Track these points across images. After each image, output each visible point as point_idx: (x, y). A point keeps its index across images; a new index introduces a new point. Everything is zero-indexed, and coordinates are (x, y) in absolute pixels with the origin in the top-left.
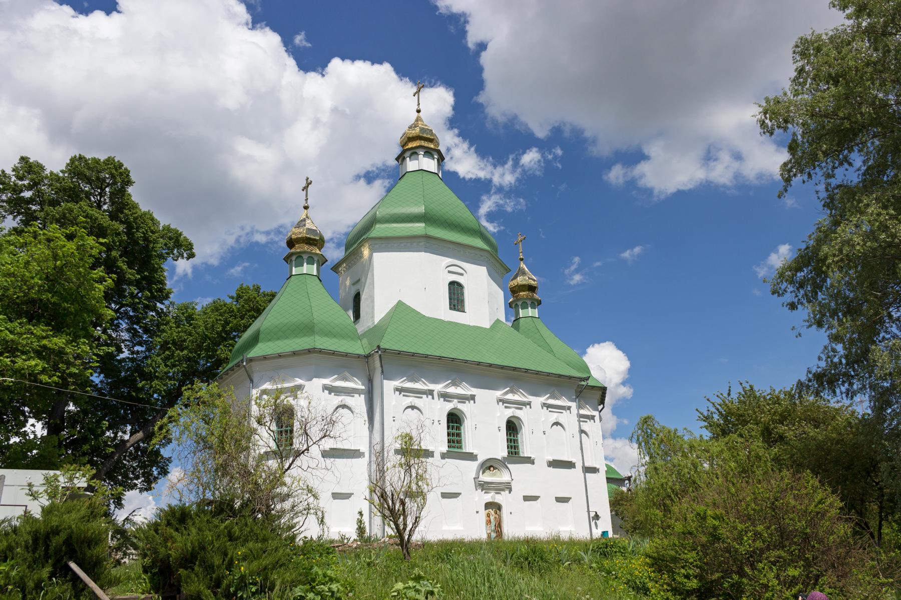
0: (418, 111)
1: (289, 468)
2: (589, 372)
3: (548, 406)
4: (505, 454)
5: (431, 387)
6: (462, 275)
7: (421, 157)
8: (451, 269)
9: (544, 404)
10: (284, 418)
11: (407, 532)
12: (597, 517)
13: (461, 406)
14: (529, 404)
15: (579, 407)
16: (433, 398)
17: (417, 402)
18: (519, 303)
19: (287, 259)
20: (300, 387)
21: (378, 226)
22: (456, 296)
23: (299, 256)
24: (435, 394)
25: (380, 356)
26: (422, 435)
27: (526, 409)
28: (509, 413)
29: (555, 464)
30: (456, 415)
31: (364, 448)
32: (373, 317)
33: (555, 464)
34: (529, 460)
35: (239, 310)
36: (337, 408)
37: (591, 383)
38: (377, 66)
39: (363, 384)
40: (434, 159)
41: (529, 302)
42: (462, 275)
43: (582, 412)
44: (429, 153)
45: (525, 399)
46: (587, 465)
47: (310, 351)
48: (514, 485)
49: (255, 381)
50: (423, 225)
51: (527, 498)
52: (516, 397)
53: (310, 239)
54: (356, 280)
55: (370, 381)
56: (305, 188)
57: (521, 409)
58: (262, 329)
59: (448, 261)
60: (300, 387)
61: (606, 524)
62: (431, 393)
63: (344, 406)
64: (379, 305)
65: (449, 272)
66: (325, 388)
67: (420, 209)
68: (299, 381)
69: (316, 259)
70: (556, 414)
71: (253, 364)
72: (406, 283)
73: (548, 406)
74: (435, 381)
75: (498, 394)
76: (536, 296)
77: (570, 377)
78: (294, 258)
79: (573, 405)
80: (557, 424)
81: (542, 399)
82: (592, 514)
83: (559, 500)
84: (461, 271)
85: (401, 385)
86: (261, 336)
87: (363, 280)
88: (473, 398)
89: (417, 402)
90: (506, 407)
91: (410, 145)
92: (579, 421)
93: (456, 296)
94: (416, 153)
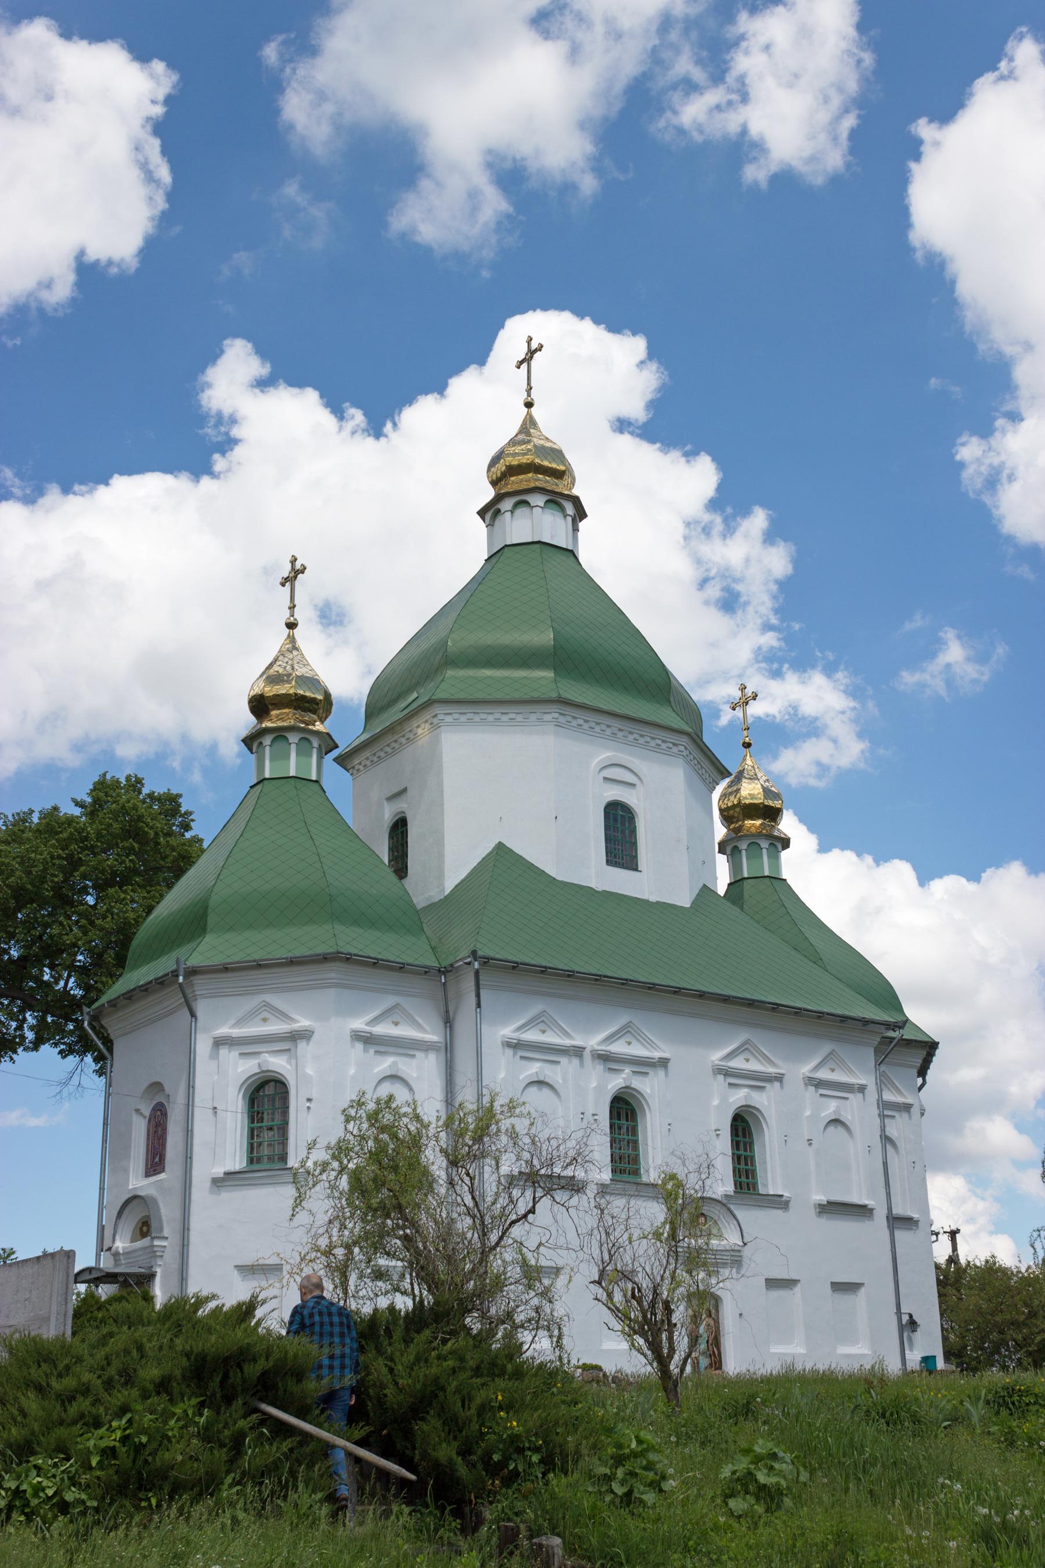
0: (529, 405)
1: (497, 1244)
2: (898, 1007)
4: (729, 1188)
5: (578, 1042)
6: (633, 785)
8: (611, 773)
10: (267, 1099)
11: (677, 1358)
12: (913, 1324)
13: (637, 1083)
14: (779, 1078)
15: (883, 1082)
17: (553, 1074)
18: (743, 845)
19: (251, 741)
20: (305, 1035)
21: (450, 673)
22: (620, 830)
23: (280, 734)
24: (587, 1054)
25: (477, 973)
26: (708, 1182)
27: (773, 1089)
28: (739, 1097)
29: (833, 1209)
30: (627, 1103)
33: (833, 1209)
34: (779, 1202)
35: (99, 836)
37: (907, 1034)
38: (947, 886)
39: (433, 1033)
40: (752, 716)
42: (633, 785)
43: (888, 1096)
45: (771, 1070)
46: (897, 1211)
47: (325, 958)
48: (746, 1252)
49: (202, 1007)
50: (550, 674)
51: (772, 1283)
52: (638, 1050)
53: (303, 697)
54: (396, 789)
55: (448, 1022)
57: (761, 1088)
58: (212, 903)
59: (606, 755)
60: (305, 1035)
61: (929, 1342)
62: (578, 1052)
63: (540, 1083)
66: (359, 1037)
67: (545, 638)
68: (303, 1023)
69: (315, 744)
70: (744, 1091)
71: (197, 980)
72: (507, 793)
73: (819, 1084)
75: (716, 1056)
77: (866, 1022)
78: (267, 740)
80: (836, 1122)
82: (905, 1319)
83: (839, 1287)
84: (629, 778)
85: (516, 1035)
86: (212, 920)
87: (410, 793)
88: (664, 1063)
89: (553, 1074)
91: (516, 482)
92: (882, 1117)
93: (620, 830)
94: (526, 503)
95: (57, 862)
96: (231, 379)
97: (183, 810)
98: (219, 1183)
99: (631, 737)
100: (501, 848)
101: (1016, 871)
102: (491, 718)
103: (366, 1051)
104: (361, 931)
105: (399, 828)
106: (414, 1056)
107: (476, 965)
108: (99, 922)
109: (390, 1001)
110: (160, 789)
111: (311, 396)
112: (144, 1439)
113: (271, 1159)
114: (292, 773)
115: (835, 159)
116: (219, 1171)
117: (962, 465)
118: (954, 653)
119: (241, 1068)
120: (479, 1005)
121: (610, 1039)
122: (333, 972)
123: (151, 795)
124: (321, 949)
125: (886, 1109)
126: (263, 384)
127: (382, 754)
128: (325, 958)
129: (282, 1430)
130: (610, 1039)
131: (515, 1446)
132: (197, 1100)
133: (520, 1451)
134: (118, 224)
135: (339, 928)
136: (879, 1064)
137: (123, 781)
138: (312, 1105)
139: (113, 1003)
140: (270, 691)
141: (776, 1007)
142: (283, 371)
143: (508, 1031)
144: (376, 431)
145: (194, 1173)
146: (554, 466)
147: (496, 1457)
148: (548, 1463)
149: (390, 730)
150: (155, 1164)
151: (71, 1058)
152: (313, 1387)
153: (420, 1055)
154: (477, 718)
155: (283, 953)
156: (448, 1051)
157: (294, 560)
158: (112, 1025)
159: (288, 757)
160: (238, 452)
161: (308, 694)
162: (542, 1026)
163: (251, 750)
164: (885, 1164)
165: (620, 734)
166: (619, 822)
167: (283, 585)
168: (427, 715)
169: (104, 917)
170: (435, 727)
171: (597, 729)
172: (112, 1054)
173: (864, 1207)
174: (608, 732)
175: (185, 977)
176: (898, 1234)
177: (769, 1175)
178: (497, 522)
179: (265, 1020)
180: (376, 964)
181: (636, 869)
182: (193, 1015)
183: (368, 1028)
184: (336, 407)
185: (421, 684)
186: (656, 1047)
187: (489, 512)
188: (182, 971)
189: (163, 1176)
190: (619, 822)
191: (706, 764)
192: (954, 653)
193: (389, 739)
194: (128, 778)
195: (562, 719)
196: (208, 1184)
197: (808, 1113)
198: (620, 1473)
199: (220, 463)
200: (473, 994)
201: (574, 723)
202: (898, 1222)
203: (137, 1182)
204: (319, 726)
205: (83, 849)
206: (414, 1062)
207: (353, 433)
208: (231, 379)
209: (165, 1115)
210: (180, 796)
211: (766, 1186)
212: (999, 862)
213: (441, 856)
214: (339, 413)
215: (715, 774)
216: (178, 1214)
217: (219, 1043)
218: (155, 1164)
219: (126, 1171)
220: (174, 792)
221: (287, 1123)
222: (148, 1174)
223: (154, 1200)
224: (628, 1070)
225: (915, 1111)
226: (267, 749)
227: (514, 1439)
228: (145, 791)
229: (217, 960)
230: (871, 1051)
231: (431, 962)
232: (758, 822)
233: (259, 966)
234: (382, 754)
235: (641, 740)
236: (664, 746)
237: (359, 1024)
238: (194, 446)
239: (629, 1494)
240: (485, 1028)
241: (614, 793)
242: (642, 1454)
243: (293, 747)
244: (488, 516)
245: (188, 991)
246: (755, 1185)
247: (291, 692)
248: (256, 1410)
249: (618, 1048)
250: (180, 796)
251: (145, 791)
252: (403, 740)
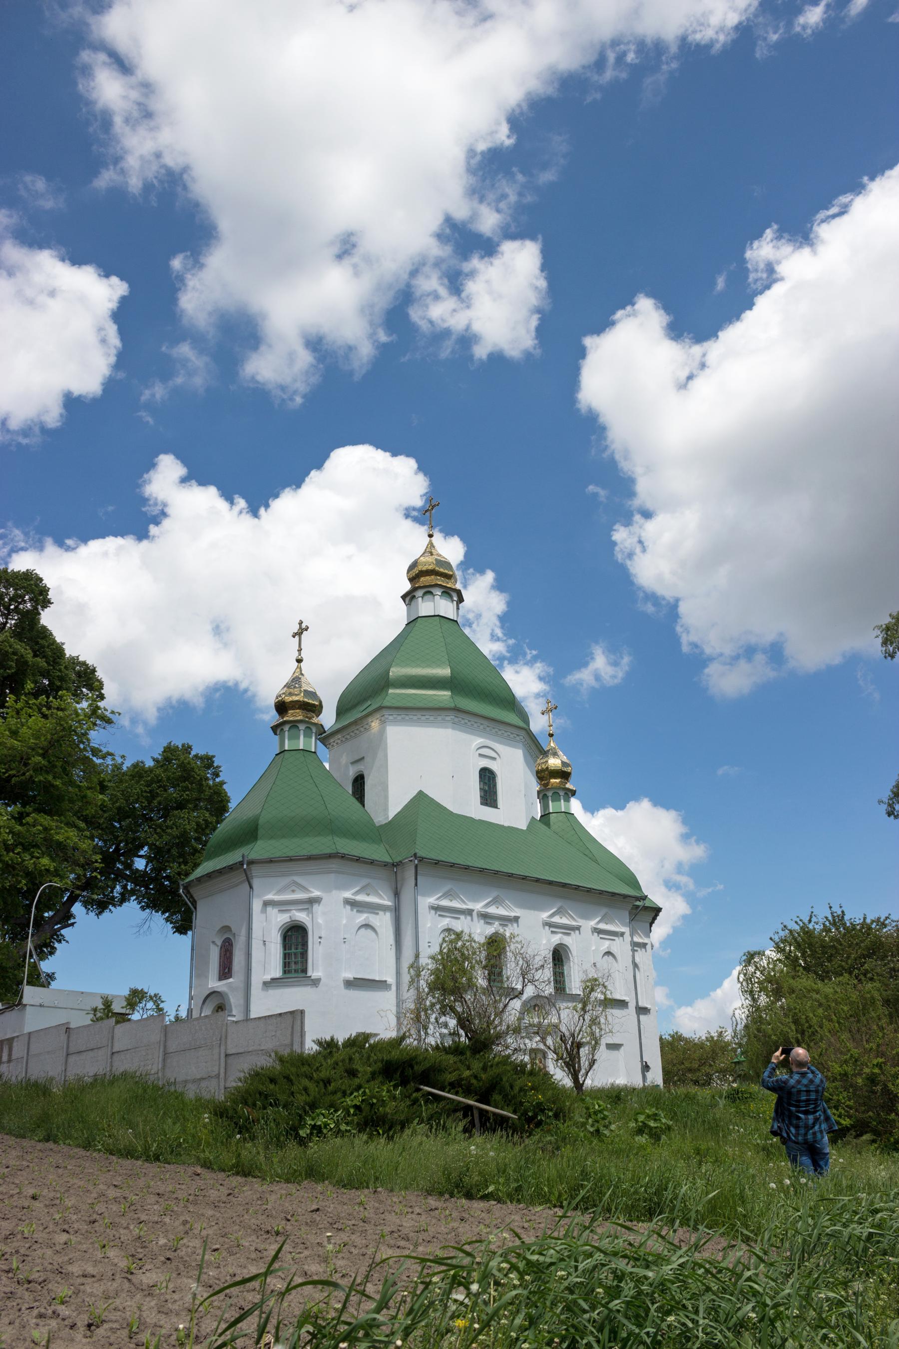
3: (600, 932)
5: (470, 906)
6: (494, 759)
7: (437, 598)
9: (595, 929)
10: (295, 938)
14: (578, 928)
16: (472, 920)
18: (550, 794)
21: (391, 691)
23: (294, 725)
24: (475, 914)
25: (416, 866)
27: (575, 935)
28: (556, 939)
31: (391, 979)
32: (386, 809)
36: (359, 929)
39: (389, 900)
40: (453, 601)
41: (562, 793)
42: (494, 759)
43: (636, 939)
44: (448, 592)
46: (641, 1004)
47: (330, 856)
49: (256, 883)
52: (502, 911)
54: (357, 758)
55: (397, 894)
56: (299, 634)
57: (568, 934)
58: (261, 822)
59: (479, 741)
60: (312, 901)
62: (469, 912)
63: (367, 926)
64: (392, 798)
65: (480, 755)
68: (316, 893)
69: (314, 731)
70: (559, 936)
73: (600, 932)
74: (476, 900)
75: (545, 915)
76: (569, 786)
77: (625, 897)
78: (286, 728)
79: (626, 930)
80: (608, 953)
81: (592, 923)
84: (493, 754)
85: (436, 902)
86: (261, 832)
87: (367, 760)
88: (516, 919)
90: (553, 932)
91: (424, 580)
92: (634, 951)
94: (431, 593)
95: (144, 794)
96: (165, 479)
97: (215, 765)
98: (267, 985)
99: (494, 731)
100: (421, 796)
101: (646, 804)
102: (415, 718)
103: (352, 910)
104: (347, 841)
105: (359, 782)
106: (377, 914)
107: (416, 862)
108: (169, 831)
109: (365, 881)
110: (202, 753)
111: (212, 491)
112: (375, 1101)
113: (296, 971)
114: (301, 747)
115: (528, 341)
116: (268, 977)
117: (614, 544)
118: (600, 662)
119: (280, 919)
120: (416, 885)
121: (487, 905)
122: (334, 864)
123: (196, 756)
124: (328, 851)
125: (636, 946)
126: (184, 480)
127: (348, 737)
128: (330, 856)
129: (438, 1098)
130: (487, 905)
131: (540, 1108)
132: (254, 936)
133: (542, 1111)
134: (89, 373)
135: (337, 839)
136: (631, 920)
137: (180, 746)
138: (322, 941)
139: (199, 880)
140: (288, 699)
141: (577, 888)
142: (197, 475)
143: (432, 900)
144: (254, 512)
145: (253, 978)
146: (446, 571)
147: (530, 1114)
148: (556, 1116)
149: (355, 723)
150: (225, 971)
151: (148, 910)
152: (450, 1077)
153: (381, 913)
154: (407, 718)
155: (305, 852)
156: (397, 912)
157: (301, 623)
158: (196, 892)
159: (299, 738)
160: (166, 523)
161: (310, 701)
162: (450, 897)
163: (276, 734)
164: (635, 977)
165: (488, 729)
166: (487, 778)
167: (294, 637)
168: (378, 715)
169: (172, 828)
170: (383, 722)
171: (475, 725)
172: (195, 908)
173: (624, 1001)
174: (482, 727)
175: (248, 865)
176: (642, 1017)
177: (293, 975)
178: (413, 603)
179: (293, 891)
180: (358, 860)
181: (496, 807)
182: (251, 887)
183: (353, 897)
184: (228, 496)
185: (369, 695)
186: (512, 910)
187: (409, 597)
188: (245, 862)
189: (231, 980)
190: (487, 778)
191: (533, 747)
192: (600, 662)
193: (353, 728)
194: (183, 745)
195: (456, 720)
196: (261, 985)
197: (594, 948)
198: (590, 1121)
199: (153, 530)
200: (414, 878)
201: (463, 722)
202: (642, 1010)
203: (214, 984)
204: (315, 720)
205: (159, 787)
206: (378, 917)
207: (241, 512)
208: (165, 479)
209: (231, 945)
210: (214, 756)
211: (570, 989)
212: (636, 798)
213: (386, 798)
214: (231, 502)
215: (537, 753)
216: (242, 1002)
217: (266, 904)
218: (225, 971)
219: (207, 977)
220: (210, 754)
221: (307, 951)
222: (220, 979)
223: (227, 994)
224: (497, 923)
225: (649, 947)
226: (287, 733)
227: (539, 1104)
228: (193, 753)
229: (266, 856)
230: (627, 913)
231: (388, 859)
232: (558, 781)
233: (290, 860)
234: (348, 737)
235: (500, 733)
236: (512, 736)
237: (348, 894)
238: (138, 520)
239: (598, 1131)
240: (420, 898)
241: (485, 763)
242: (601, 1112)
243: (302, 732)
244: (407, 599)
245: (248, 873)
246: (564, 989)
247: (301, 699)
248: (421, 1090)
249: (492, 910)
250: (214, 756)
251: (193, 753)
252: (362, 729)
